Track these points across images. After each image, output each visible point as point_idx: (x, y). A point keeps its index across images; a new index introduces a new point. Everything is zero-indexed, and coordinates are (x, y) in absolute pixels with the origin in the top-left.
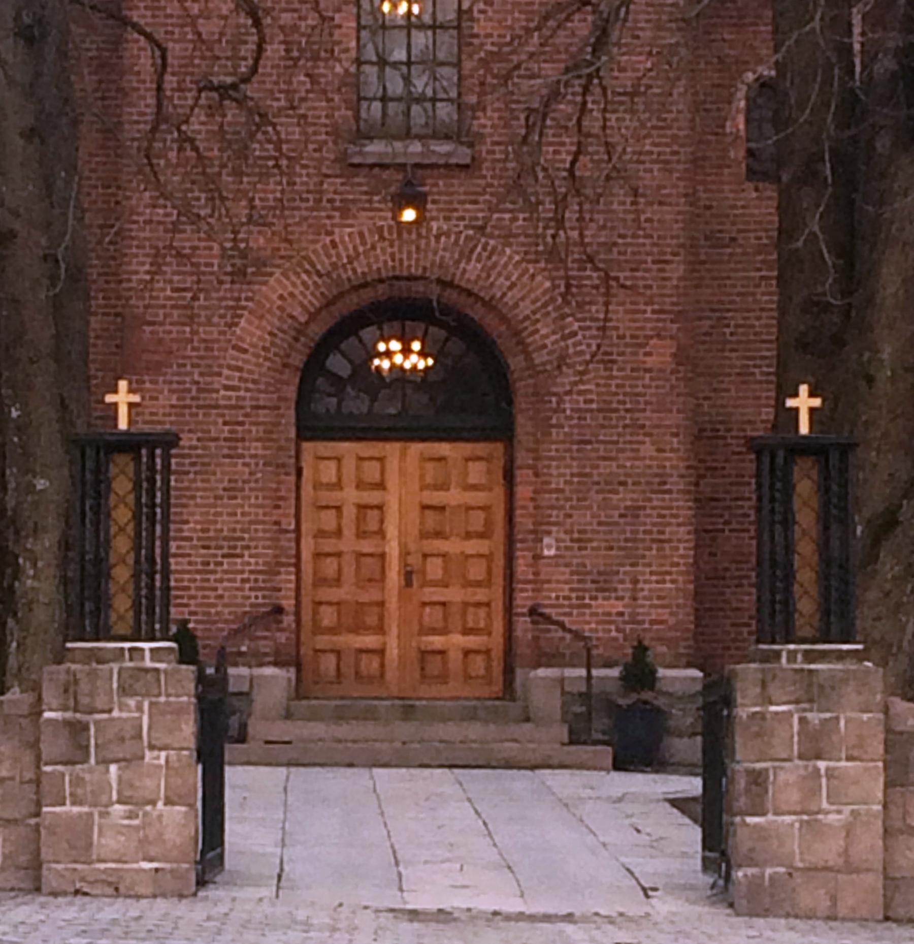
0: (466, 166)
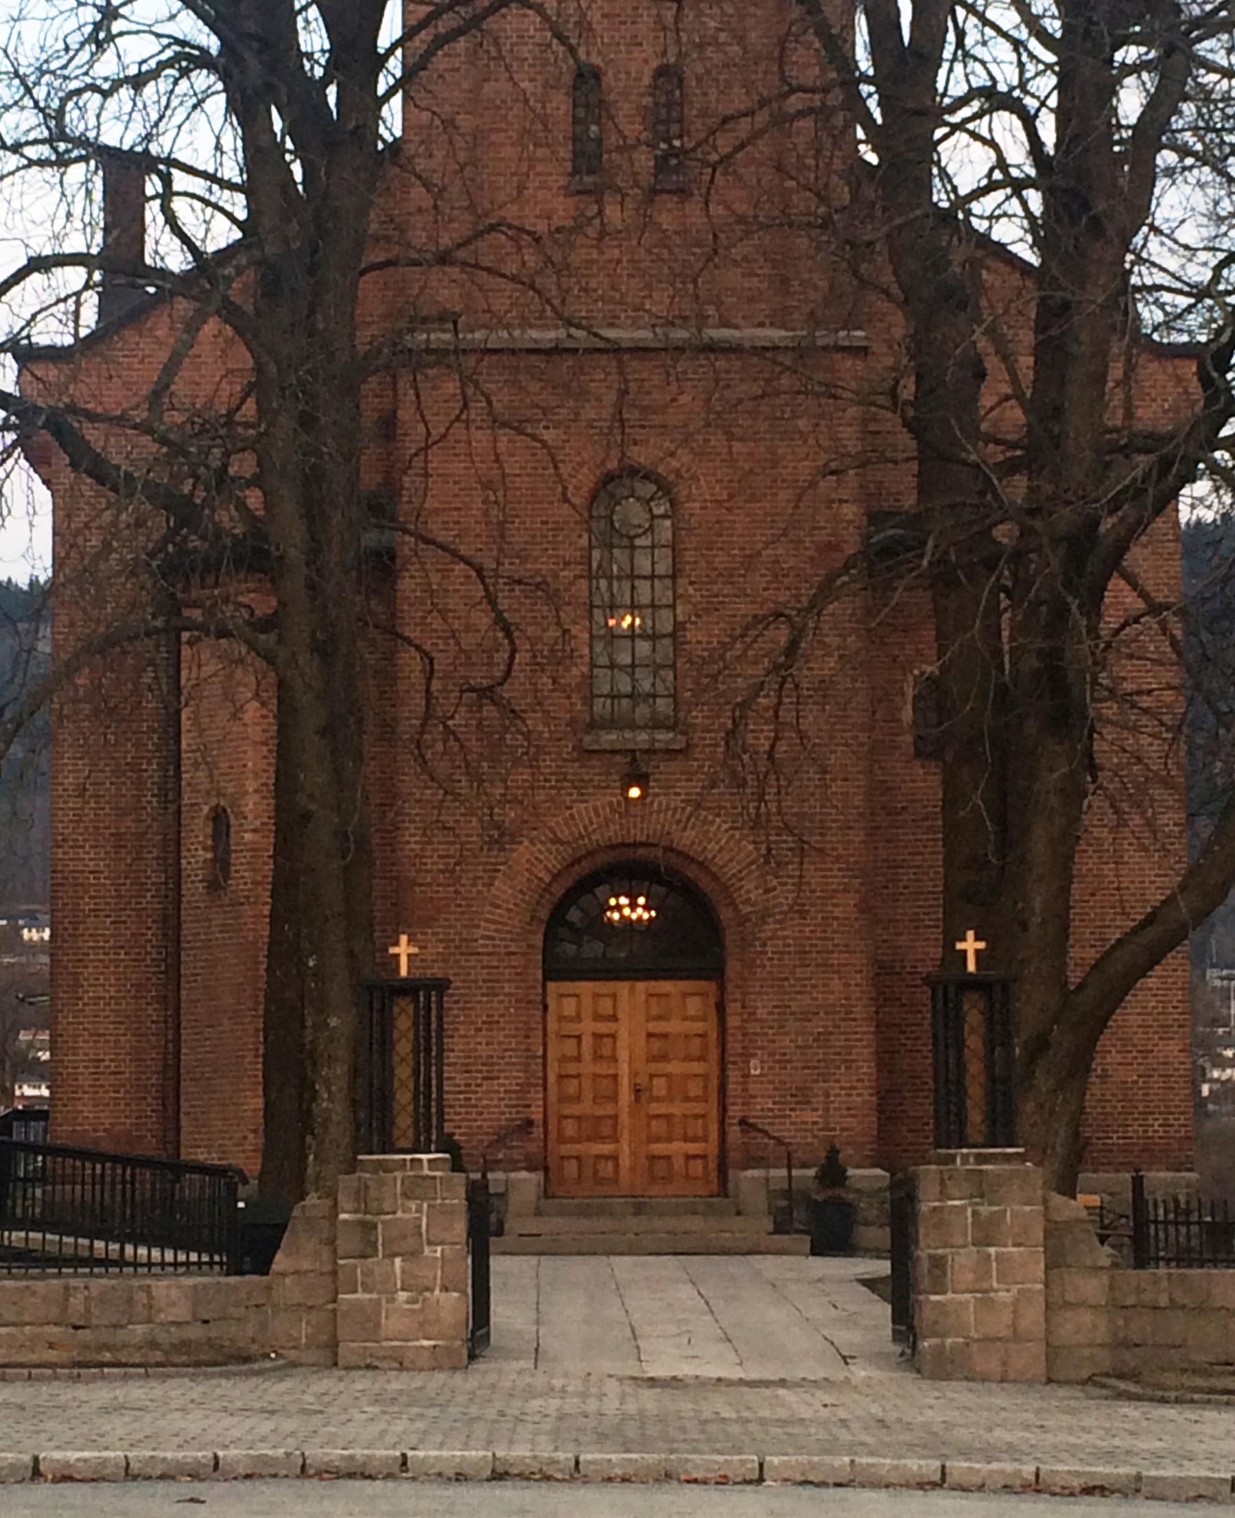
0: (681, 751)
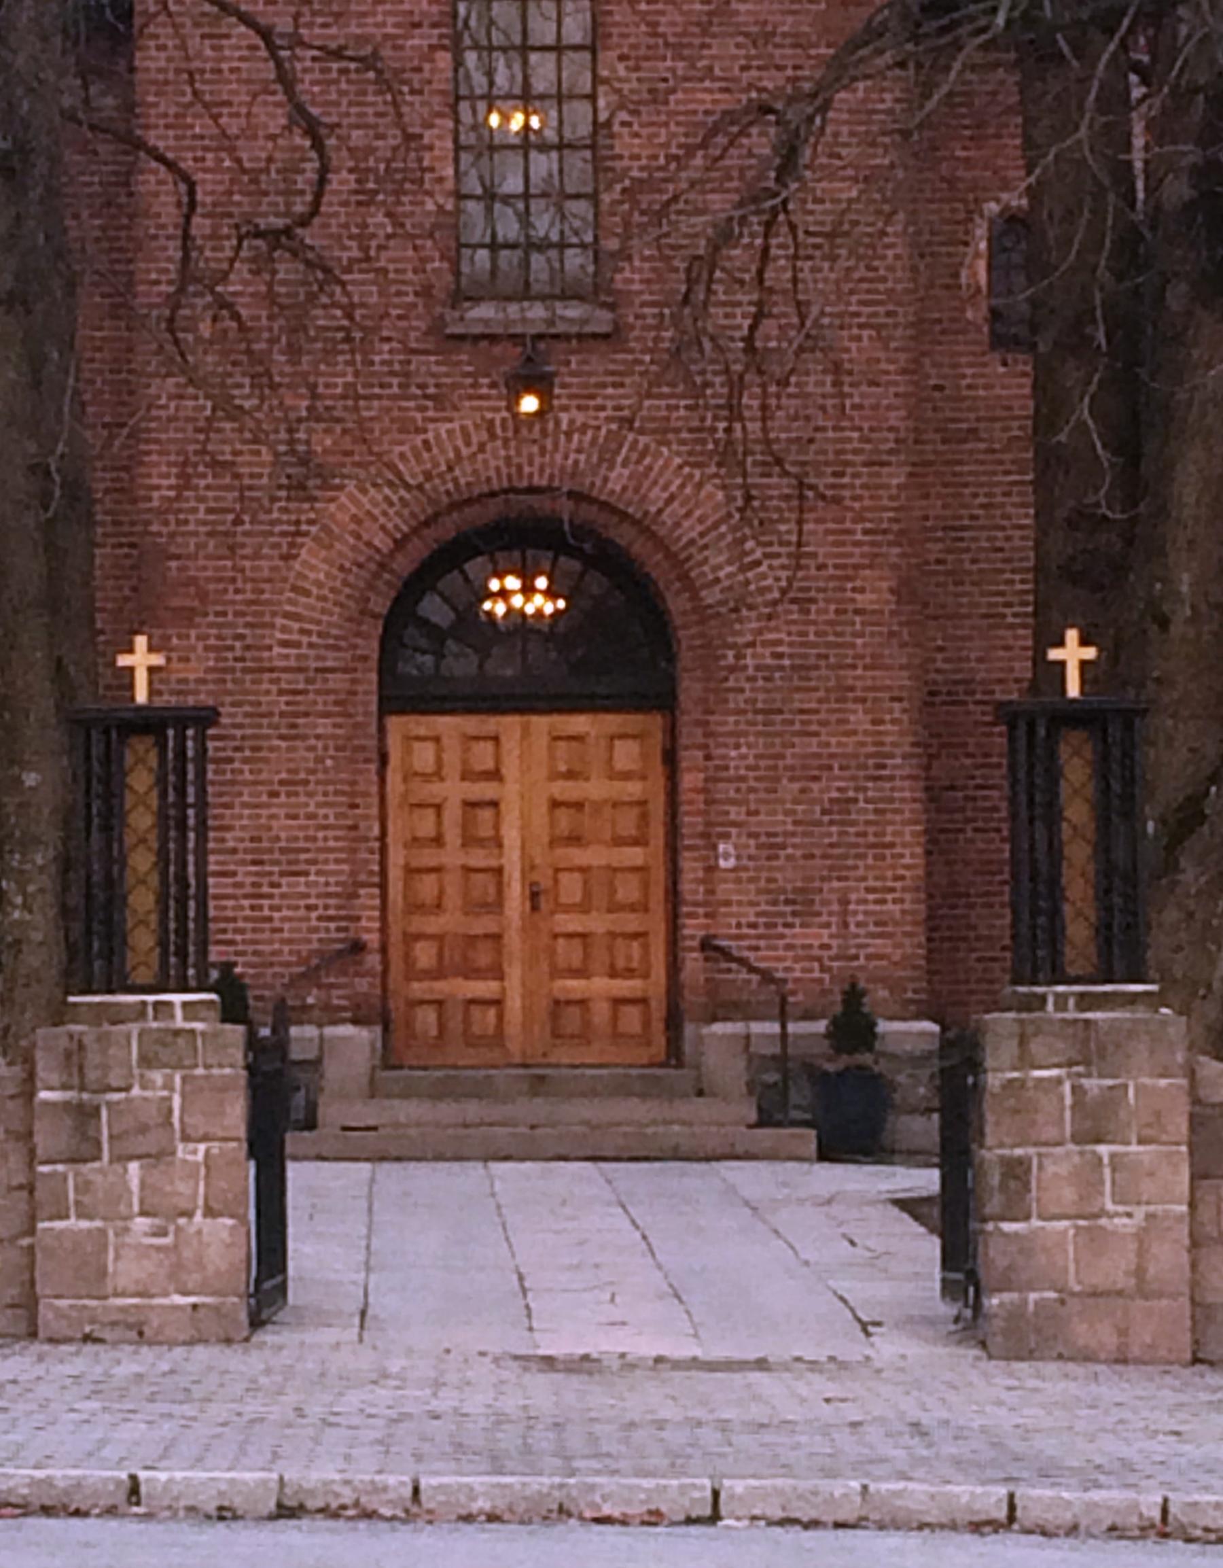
0: (606, 336)
